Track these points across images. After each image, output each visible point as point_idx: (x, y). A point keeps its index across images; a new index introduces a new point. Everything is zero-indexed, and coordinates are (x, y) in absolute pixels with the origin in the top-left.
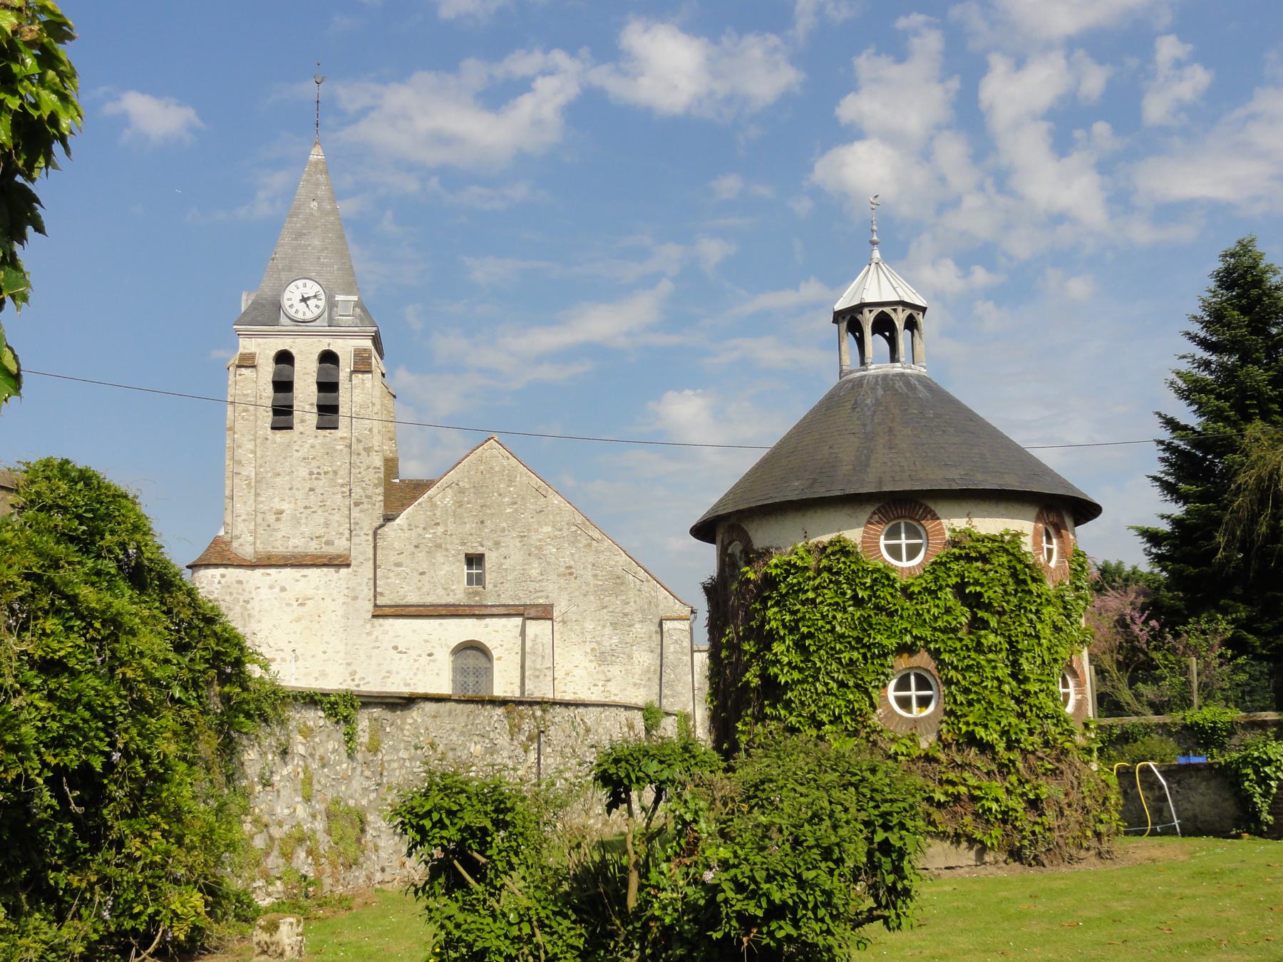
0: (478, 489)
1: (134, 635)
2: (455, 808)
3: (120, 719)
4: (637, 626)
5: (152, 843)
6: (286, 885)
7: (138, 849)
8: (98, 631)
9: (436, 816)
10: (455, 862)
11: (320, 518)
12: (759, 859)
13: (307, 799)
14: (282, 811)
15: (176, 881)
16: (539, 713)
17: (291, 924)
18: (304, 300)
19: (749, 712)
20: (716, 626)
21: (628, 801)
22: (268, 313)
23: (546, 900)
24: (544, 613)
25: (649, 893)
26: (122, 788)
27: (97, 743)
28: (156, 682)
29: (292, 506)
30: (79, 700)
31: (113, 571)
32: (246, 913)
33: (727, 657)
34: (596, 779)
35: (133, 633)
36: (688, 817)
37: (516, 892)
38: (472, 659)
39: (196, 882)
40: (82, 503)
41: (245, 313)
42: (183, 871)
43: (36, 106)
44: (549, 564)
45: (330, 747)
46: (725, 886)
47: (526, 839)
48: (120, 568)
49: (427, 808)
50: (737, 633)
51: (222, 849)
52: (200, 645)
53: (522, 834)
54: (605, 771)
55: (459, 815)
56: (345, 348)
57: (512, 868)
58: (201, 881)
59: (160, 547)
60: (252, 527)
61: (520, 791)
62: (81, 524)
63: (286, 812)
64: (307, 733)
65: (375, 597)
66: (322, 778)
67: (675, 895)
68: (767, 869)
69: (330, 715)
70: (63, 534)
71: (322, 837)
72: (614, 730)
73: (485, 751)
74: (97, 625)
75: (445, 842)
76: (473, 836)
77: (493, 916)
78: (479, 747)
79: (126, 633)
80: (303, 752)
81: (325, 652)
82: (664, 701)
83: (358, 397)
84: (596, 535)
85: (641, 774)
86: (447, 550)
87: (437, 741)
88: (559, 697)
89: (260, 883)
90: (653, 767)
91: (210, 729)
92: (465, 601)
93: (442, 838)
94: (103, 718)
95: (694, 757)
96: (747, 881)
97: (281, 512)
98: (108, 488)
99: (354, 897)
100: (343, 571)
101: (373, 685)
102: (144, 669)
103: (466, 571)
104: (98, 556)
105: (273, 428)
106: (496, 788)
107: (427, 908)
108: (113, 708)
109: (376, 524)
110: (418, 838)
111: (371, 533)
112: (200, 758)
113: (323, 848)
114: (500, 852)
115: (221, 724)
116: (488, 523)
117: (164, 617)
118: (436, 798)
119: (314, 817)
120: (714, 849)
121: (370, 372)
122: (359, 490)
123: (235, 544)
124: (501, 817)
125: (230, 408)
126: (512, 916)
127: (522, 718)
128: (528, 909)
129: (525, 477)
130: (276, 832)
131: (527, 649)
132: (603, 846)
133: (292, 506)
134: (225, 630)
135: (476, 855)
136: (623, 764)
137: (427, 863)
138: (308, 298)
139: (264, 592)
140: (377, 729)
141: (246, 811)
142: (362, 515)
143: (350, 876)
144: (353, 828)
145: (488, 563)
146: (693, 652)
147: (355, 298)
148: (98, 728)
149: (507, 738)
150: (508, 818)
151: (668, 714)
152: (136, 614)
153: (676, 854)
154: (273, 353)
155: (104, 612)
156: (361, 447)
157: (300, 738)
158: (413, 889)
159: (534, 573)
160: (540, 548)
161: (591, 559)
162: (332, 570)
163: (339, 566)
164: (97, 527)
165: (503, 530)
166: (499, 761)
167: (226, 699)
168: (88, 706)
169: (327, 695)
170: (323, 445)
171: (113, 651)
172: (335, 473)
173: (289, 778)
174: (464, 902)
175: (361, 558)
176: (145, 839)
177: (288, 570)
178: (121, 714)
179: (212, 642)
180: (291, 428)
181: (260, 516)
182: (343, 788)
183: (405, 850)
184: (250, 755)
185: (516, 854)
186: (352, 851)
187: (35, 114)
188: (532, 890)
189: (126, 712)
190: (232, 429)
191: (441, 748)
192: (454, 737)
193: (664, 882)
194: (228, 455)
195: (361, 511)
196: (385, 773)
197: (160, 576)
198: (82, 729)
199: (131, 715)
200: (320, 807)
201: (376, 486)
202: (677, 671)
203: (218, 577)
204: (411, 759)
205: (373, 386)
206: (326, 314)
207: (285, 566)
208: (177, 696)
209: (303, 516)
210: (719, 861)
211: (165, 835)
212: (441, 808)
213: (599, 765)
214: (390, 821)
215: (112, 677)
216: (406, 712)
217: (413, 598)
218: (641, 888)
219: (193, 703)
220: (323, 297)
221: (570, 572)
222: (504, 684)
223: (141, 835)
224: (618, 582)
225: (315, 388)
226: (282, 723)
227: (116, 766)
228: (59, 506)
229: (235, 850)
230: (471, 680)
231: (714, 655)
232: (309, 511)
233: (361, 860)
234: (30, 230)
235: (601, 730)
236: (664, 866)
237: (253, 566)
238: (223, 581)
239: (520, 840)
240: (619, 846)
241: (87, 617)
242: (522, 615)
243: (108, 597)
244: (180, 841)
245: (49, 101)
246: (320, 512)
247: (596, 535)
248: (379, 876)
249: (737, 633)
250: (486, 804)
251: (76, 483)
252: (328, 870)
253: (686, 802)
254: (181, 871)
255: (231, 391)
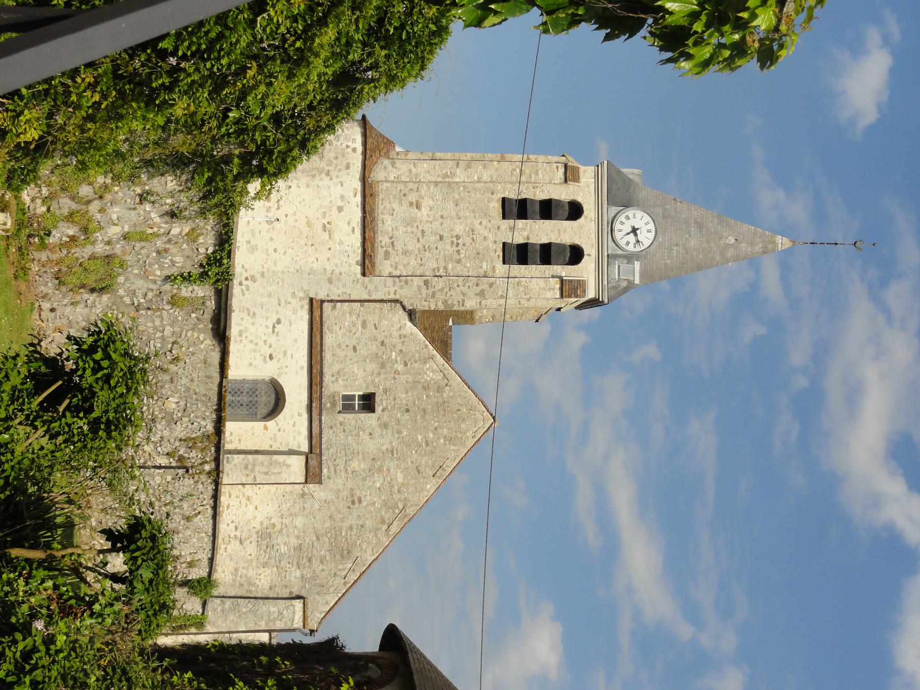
0: (442, 406)
1: (288, 78)
2: (113, 382)
3: (208, 65)
4: (298, 573)
5: (88, 93)
6: (42, 216)
7: (83, 80)
8: (293, 44)
9: (105, 364)
10: (60, 382)
11: (413, 246)
12: (54, 673)
13: (126, 237)
14: (115, 212)
15: (50, 116)
16: (207, 467)
17: (5, 224)
18: (634, 231)
19: (203, 685)
20: (293, 651)
21: (114, 549)
22: (620, 195)
23: (20, 469)
24: (313, 475)
25: (24, 569)
26: (143, 65)
27: (186, 44)
28: (243, 94)
29: (425, 219)
30: (227, 28)
31: (350, 57)
32: (16, 179)
33: (260, 662)
34: (136, 517)
35: (291, 76)
36: (97, 607)
37: (29, 441)
38: (266, 400)
39: (49, 133)
40: (416, 29)
41: (619, 172)
42: (60, 121)
43: (696, 44)
44: (364, 479)
45: (177, 259)
46: (29, 640)
47: (80, 450)
48: (353, 63)
49: (114, 356)
50: (284, 673)
51: (80, 157)
52: (279, 135)
53: (85, 446)
54: (144, 527)
55: (106, 387)
56: (586, 270)
57: (53, 437)
58: (50, 138)
59: (374, 100)
60: (403, 179)
61: (127, 445)
62: (395, 28)
63: (114, 217)
64: (192, 237)
65: (331, 301)
66: (147, 251)
67: (21, 594)
68: (44, 682)
69: (209, 259)
70: (386, 13)
71: (88, 250)
72: (187, 548)
73: (170, 412)
74: (298, 44)
75: (79, 373)
76: (85, 399)
77: (8, 418)
78: (174, 406)
79: (290, 70)
80: (172, 232)
81: (275, 250)
82: (218, 601)
83: (536, 285)
84: (394, 529)
85: (140, 562)
86: (379, 374)
87: (181, 364)
88: (224, 490)
89: (45, 191)
90: (146, 574)
91: (198, 145)
92: (326, 392)
93: (84, 370)
94: (210, 50)
95: (155, 614)
96: (33, 662)
97: (418, 207)
98: (431, 52)
99: (27, 281)
100: (358, 269)
101: (238, 299)
102: (255, 87)
103: (357, 394)
104: (365, 44)
105: (504, 199)
106: (130, 420)
107: (18, 355)
108: (219, 59)
109: (406, 303)
110: (85, 347)
111: (397, 297)
112: (169, 135)
113: (77, 252)
114: (69, 425)
115: (202, 155)
116: (407, 416)
117: (304, 104)
118: (122, 364)
119: (109, 243)
120: (65, 630)
121: (562, 296)
122: (441, 285)
123: (386, 162)
124: (103, 426)
125: (519, 157)
126: (6, 436)
127: (202, 450)
128: (12, 452)
129: (454, 454)
130: (94, 207)
131: (275, 457)
132: (69, 526)
133: (425, 219)
134: (294, 159)
135: (67, 402)
136: (150, 544)
137: (60, 354)
138: (636, 235)
139: (337, 191)
140: (195, 305)
141: (117, 178)
142: (415, 288)
143: (48, 278)
144: (96, 281)
145: (364, 416)
146: (270, 631)
147: (637, 281)
148: (200, 44)
149: (182, 435)
150: (101, 433)
151: (204, 605)
152: (308, 79)
153: (61, 595)
154: (579, 199)
155: (310, 49)
156: (485, 287)
157: (187, 229)
158: (36, 341)
159: (355, 465)
160: (380, 470)
161: (369, 523)
162: (359, 258)
163: (363, 265)
164: (393, 43)
165: (399, 432)
166: (159, 427)
167: (227, 160)
168: (221, 36)
169: (229, 256)
170: (487, 249)
171: (273, 58)
172: (459, 261)
173: (147, 219)
174: (20, 391)
175: (371, 287)
176: (92, 86)
177: (359, 214)
178: (213, 66)
179: (282, 147)
180: (504, 218)
181: (415, 186)
182: (136, 271)
183: (73, 333)
184: (170, 183)
185: (65, 441)
186: (73, 280)
187: (690, 42)
188: (30, 456)
189: (215, 69)
190: (503, 159)
191: (173, 368)
192: (184, 381)
193: (34, 584)
194: (477, 156)
195: (419, 288)
196: (149, 312)
197: (346, 100)
198: (199, 30)
199: (212, 75)
200: (118, 249)
201: (445, 302)
202: (250, 616)
203: (354, 145)
204: (163, 338)
205: (547, 299)
206: (620, 252)
207: (364, 211)
208: (231, 115)
209: (414, 229)
210: (53, 636)
211: (96, 105)
212: (113, 370)
213: (149, 520)
214: (102, 320)
215: (248, 57)
216: (210, 333)
217: (329, 340)
218: (29, 561)
219: (223, 130)
220: (638, 249)
221: (355, 501)
222: (238, 432)
223: (97, 83)
224: (343, 552)
225: (545, 240)
226: (202, 213)
227: (163, 60)
228: (413, 8)
229: (80, 170)
230: (244, 399)
231: (262, 649)
232: (419, 234)
233: (64, 289)
234: (604, 32)
235: (188, 532)
236: (49, 584)
237: (364, 180)
238: (349, 150)
239: (79, 445)
240: (68, 541)
241: (307, 35)
242: (311, 451)
243: (324, 54)
244: (90, 118)
245: (705, 52)
246: (419, 245)
247: (394, 529)
248: (46, 306)
249: (284, 673)
250: (116, 412)
251: (435, 24)
252: (55, 257)
253: (112, 605)
254: (60, 120)
255: (541, 158)
